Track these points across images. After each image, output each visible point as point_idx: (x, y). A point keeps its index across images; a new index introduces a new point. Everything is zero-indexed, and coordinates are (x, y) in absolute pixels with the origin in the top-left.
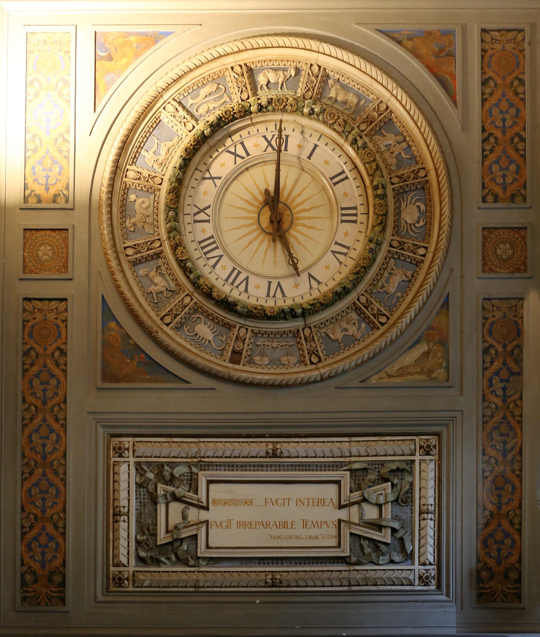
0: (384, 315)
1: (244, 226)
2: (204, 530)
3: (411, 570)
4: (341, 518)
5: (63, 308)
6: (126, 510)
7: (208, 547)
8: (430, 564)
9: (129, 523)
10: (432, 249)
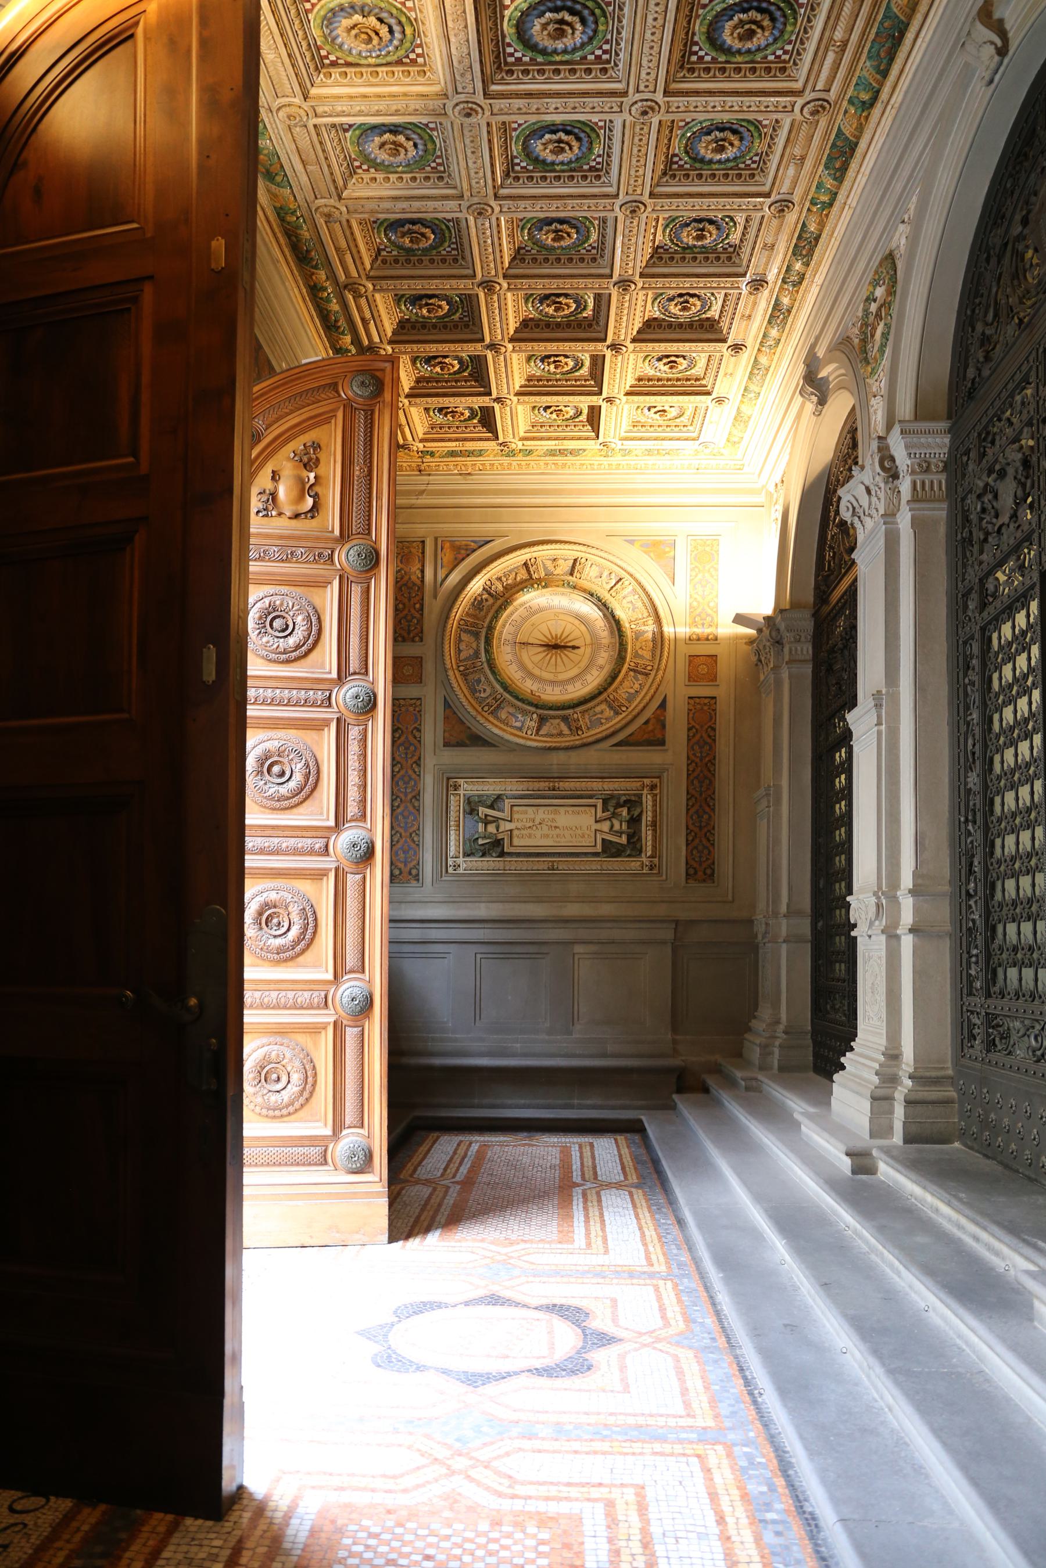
7: (595, 806)
10: (630, 709)
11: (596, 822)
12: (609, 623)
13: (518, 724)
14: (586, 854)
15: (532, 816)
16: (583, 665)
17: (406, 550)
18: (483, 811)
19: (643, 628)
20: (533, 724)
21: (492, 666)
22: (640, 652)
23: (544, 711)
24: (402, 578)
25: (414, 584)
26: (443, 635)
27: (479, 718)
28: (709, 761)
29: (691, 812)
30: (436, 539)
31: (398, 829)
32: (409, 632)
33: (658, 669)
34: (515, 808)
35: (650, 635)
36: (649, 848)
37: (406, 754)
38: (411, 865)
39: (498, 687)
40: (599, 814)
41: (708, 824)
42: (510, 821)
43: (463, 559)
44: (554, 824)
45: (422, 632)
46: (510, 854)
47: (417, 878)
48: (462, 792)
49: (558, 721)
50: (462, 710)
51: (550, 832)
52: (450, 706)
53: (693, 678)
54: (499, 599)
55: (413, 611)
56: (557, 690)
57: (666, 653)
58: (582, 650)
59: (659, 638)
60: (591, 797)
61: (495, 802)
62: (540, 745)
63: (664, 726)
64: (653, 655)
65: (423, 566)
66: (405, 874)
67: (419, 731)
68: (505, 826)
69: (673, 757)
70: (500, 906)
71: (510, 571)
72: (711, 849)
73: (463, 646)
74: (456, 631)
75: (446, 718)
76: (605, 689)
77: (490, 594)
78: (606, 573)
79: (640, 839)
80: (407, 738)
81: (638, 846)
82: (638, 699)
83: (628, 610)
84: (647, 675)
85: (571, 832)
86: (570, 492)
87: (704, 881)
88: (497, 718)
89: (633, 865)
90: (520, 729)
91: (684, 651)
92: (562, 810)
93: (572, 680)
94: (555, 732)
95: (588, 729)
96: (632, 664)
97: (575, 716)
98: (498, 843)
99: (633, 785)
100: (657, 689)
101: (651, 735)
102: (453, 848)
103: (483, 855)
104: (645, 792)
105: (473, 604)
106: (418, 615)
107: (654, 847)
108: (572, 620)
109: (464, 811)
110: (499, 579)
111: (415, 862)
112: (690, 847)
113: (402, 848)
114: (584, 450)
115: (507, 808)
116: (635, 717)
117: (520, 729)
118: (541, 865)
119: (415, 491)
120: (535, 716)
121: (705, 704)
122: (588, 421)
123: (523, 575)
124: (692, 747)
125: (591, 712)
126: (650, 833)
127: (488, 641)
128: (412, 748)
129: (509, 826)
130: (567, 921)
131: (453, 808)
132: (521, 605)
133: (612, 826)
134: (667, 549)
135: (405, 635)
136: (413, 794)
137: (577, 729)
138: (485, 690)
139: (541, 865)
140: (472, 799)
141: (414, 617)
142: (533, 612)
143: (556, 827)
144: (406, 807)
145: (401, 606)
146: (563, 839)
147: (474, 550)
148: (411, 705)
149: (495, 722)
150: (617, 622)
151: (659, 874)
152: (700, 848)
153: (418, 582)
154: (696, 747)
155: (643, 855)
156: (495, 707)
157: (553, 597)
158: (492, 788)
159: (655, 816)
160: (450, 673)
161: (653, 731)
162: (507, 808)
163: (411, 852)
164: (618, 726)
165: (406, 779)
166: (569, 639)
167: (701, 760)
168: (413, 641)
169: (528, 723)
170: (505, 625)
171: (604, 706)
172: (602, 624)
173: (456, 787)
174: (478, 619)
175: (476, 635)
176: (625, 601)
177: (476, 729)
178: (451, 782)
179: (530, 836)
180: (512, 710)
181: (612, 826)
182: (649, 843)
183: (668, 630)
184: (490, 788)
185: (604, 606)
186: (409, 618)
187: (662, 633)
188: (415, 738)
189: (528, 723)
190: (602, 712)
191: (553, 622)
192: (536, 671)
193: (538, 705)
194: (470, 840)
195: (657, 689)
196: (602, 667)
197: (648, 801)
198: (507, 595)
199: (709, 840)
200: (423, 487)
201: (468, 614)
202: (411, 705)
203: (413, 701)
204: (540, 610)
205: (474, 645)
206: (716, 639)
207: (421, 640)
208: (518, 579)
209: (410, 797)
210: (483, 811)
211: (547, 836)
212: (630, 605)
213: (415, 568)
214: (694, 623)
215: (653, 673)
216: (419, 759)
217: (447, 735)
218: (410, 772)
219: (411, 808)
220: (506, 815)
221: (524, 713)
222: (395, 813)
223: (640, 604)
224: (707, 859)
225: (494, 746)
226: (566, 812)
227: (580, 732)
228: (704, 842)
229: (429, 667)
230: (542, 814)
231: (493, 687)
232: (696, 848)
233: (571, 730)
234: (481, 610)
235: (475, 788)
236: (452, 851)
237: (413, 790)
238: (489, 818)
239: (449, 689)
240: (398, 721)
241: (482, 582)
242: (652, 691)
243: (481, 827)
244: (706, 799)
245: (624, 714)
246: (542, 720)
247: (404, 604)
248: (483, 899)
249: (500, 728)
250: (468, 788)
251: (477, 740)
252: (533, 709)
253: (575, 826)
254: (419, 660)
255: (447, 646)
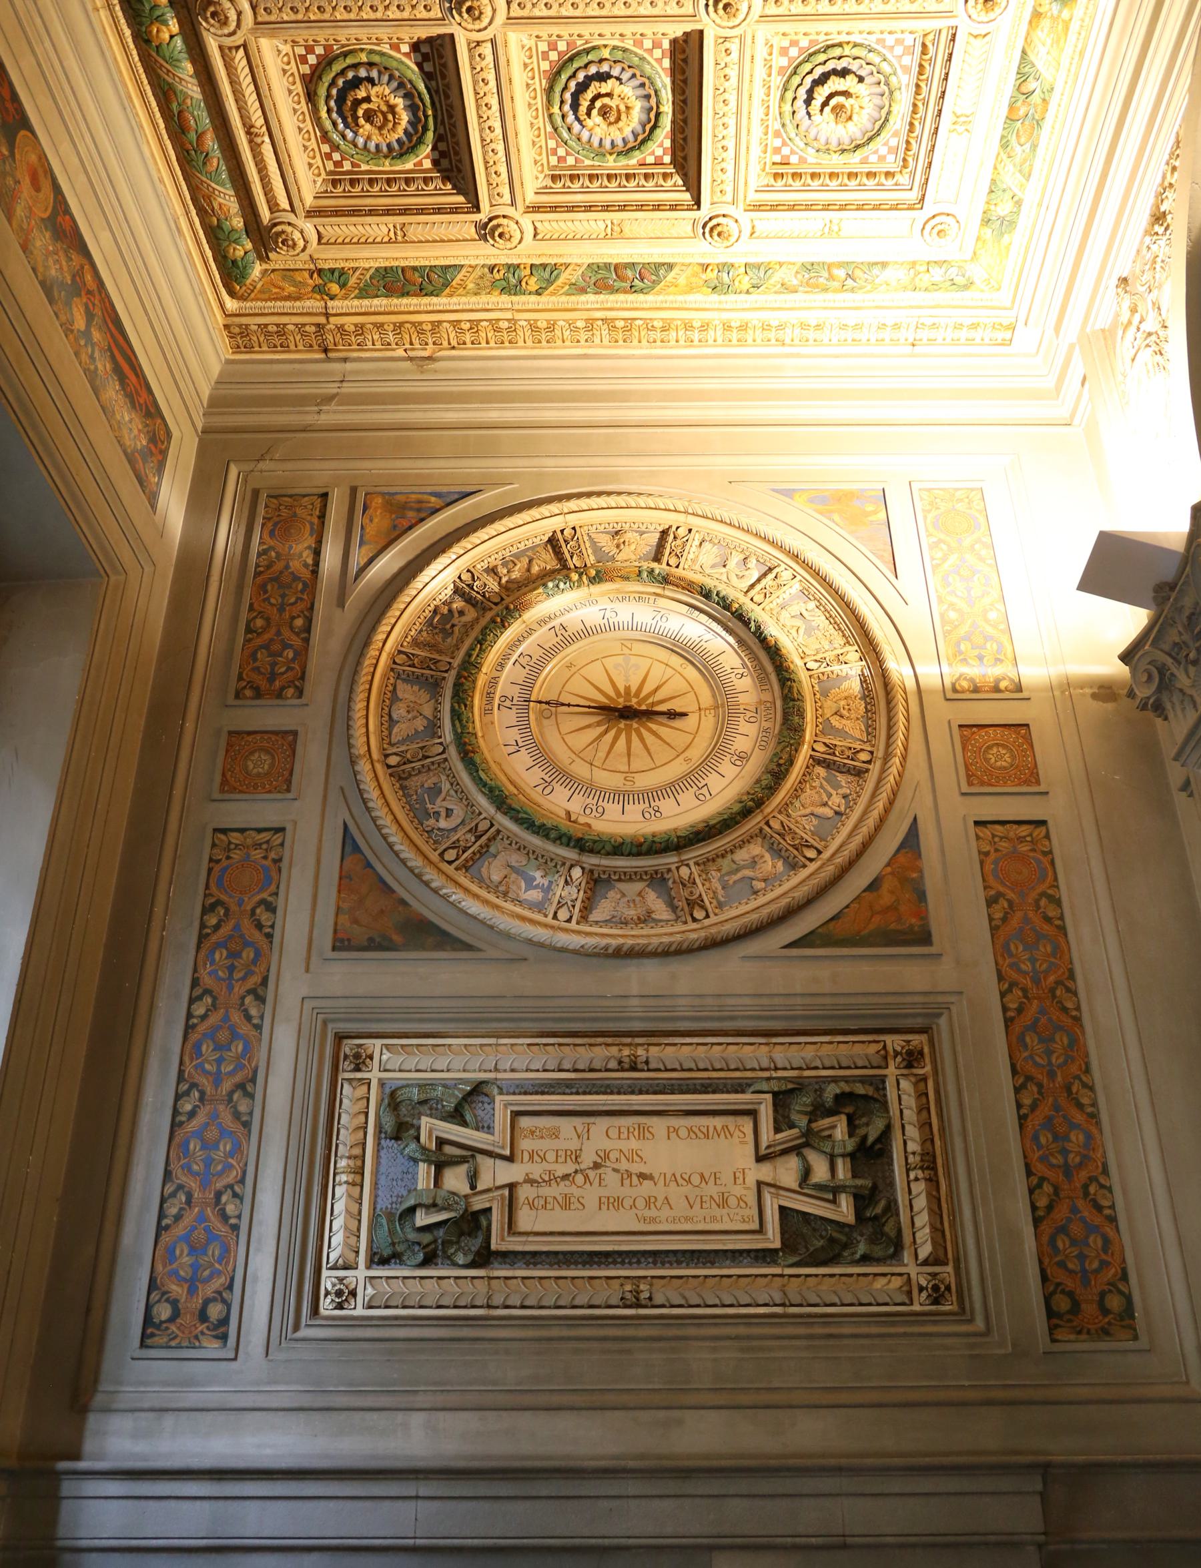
0: (812, 846)
1: (589, 726)
2: (764, 1143)
3: (385, 1070)
4: (762, 1179)
5: (279, 841)
6: (912, 1176)
7: (753, 1114)
8: (350, 1080)
9: (906, 1152)
10: (826, 855)
11: (760, 1159)
12: (754, 658)
13: (534, 895)
14: (735, 1256)
15: (574, 1145)
16: (697, 753)
17: (285, 513)
18: (430, 1127)
19: (836, 668)
20: (571, 892)
21: (468, 753)
22: (835, 721)
23: (606, 861)
24: (268, 567)
25: (296, 578)
26: (353, 682)
27: (430, 874)
28: (1058, 983)
29: (1035, 1121)
30: (354, 491)
31: (183, 1179)
32: (272, 677)
33: (887, 756)
34: (525, 1122)
35: (855, 686)
36: (924, 1234)
37: (231, 969)
38: (209, 1290)
39: (482, 801)
40: (767, 1135)
41: (1085, 1160)
42: (510, 1159)
43: (410, 528)
44: (636, 1168)
45: (303, 678)
46: (508, 1257)
47: (220, 1330)
48: (374, 1075)
49: (639, 886)
50: (388, 858)
51: (626, 1191)
52: (357, 849)
53: (978, 777)
54: (489, 607)
55: (286, 633)
56: (634, 810)
57: (901, 719)
58: (692, 721)
59: (880, 691)
60: (739, 1087)
61: (468, 1102)
62: (590, 941)
63: (922, 896)
64: (870, 730)
65: (319, 542)
66: (186, 1319)
67: (271, 909)
68: (495, 1173)
69: (963, 962)
70: (469, 1421)
71: (517, 556)
72: (1109, 1230)
73: (399, 712)
74: (385, 677)
75: (344, 879)
76: (759, 803)
77: (469, 600)
78: (736, 559)
79: (891, 1208)
80: (237, 927)
81: (889, 1228)
82: (845, 831)
83: (801, 631)
84: (859, 773)
85: (687, 1189)
86: (645, 396)
87: (1105, 1332)
88: (481, 881)
89: (883, 1284)
90: (539, 907)
91: (942, 715)
92: (658, 1125)
93: (672, 789)
94: (632, 913)
95: (720, 905)
96: (820, 748)
97: (684, 872)
98: (471, 1223)
99: (863, 1049)
100: (891, 803)
101: (894, 917)
102: (337, 1239)
103: (427, 1262)
104: (892, 1071)
105: (430, 622)
106: (297, 642)
107: (937, 1231)
108: (663, 655)
109: (379, 1129)
110: (492, 571)
111: (219, 1282)
112: (1046, 1227)
113: (187, 1238)
114: (670, 266)
115: (501, 1118)
116: (844, 871)
117: (539, 907)
118: (601, 1288)
119: (315, 396)
120: (577, 873)
121: (1021, 839)
122: (674, 162)
123: (547, 561)
124: (1006, 947)
125: (725, 863)
126: (919, 1188)
127: (461, 695)
128: (248, 954)
129: (507, 1173)
130: (684, 1473)
131: (346, 1120)
132: (542, 622)
133: (806, 1172)
134: (870, 508)
135: (263, 684)
136: (238, 1078)
137: (691, 904)
138: (449, 813)
139: (601, 1288)
140: (402, 1095)
141: (286, 646)
142: (567, 638)
143: (642, 1176)
144: (214, 1116)
145: (259, 623)
146: (665, 1213)
147: (436, 511)
148: (258, 846)
149: (474, 888)
150: (773, 652)
151: (963, 1313)
152: (1076, 1229)
153: (306, 574)
154: (1018, 948)
155: (907, 1256)
156: (474, 851)
157: (617, 606)
158: (458, 1063)
159: (928, 1140)
160: (364, 766)
161: (892, 908)
162: (501, 1118)
163: (215, 1250)
164: (799, 894)
165: (223, 1036)
166: (659, 696)
167: (1037, 982)
168: (279, 695)
169: (559, 891)
170: (502, 666)
171: (756, 849)
172: (737, 662)
173: (360, 1061)
174: (440, 652)
175: (434, 687)
176: (785, 615)
177: (425, 906)
178: (348, 1046)
179: (566, 1203)
180: (516, 859)
181: (806, 1172)
182: (922, 1219)
183: (898, 668)
184: (453, 1062)
185: (736, 619)
186: (276, 647)
187: (884, 675)
188: (259, 926)
189: (559, 891)
190: (754, 862)
191: (620, 659)
192: (580, 769)
193: (584, 844)
194: (390, 1215)
195: (891, 803)
196: (743, 757)
197: (901, 1094)
198: (507, 600)
199: (1099, 1208)
200: (332, 389)
201: (415, 643)
202: (258, 846)
203: (265, 836)
204: (587, 632)
205: (427, 710)
206: (1019, 688)
207: (300, 693)
208: (535, 569)
209: (227, 1086)
210: (430, 1127)
211: (617, 1203)
212: (798, 622)
213: (301, 549)
214: (959, 656)
215: (875, 768)
216: (265, 982)
217: (344, 919)
218: (236, 1017)
219: (226, 1118)
220: (497, 1139)
221: (550, 865)
222: (180, 1134)
223: (820, 620)
224: (1104, 1264)
225: (469, 947)
226: (672, 1131)
227: (699, 914)
228: (1087, 1212)
229: (312, 756)
230: (601, 1137)
231: (470, 805)
232: (1063, 1230)
233: (674, 909)
234: (447, 634)
235: (411, 1063)
236: (336, 1244)
237: (239, 1067)
238: (448, 1149)
239: (358, 808)
240: (220, 885)
241: (450, 575)
242: (880, 805)
243: (424, 1174)
244: (1068, 1088)
245: (812, 867)
246: (597, 883)
247: (268, 620)
248: (420, 1400)
249: (486, 902)
250: (391, 1063)
251: (425, 934)
252: (570, 854)
253: (700, 1175)
254: (290, 738)
255: (359, 705)
